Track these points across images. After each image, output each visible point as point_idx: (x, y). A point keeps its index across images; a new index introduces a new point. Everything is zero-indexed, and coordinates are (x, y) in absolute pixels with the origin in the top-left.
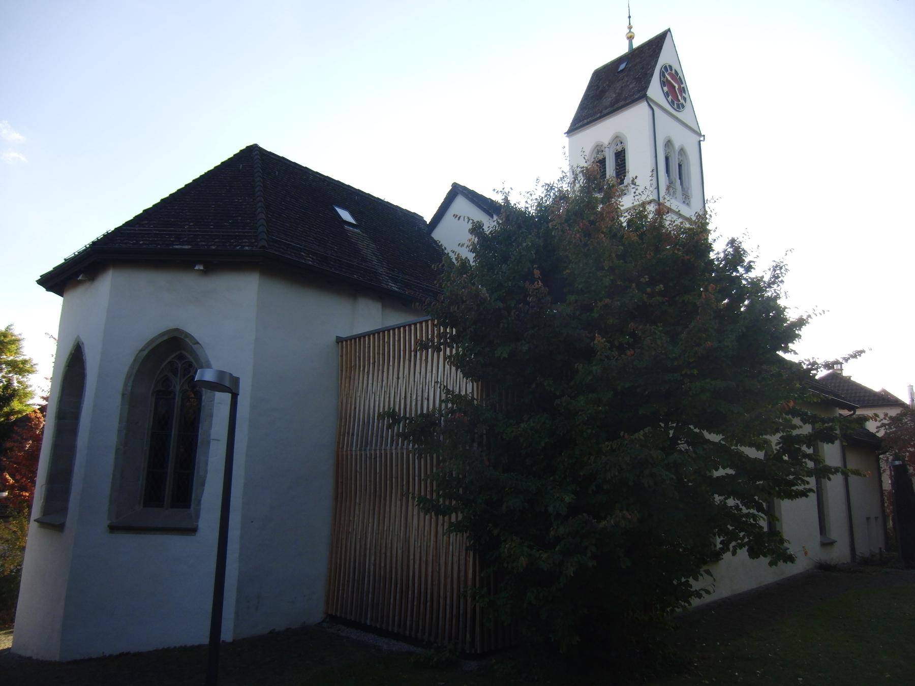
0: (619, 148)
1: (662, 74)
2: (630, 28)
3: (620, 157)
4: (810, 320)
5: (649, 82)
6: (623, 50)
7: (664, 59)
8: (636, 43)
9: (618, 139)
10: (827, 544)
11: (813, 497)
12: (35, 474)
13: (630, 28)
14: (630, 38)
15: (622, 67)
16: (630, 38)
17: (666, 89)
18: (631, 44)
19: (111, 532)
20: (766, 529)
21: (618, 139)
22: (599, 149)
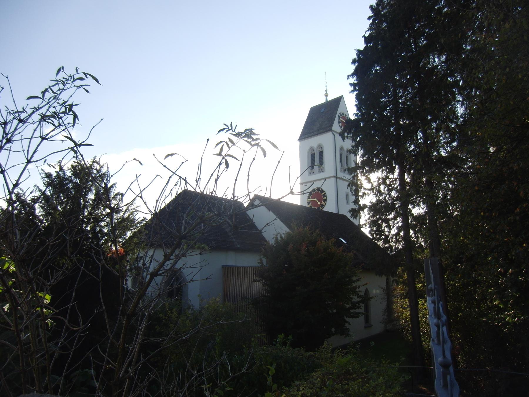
0: (321, 150)
1: (339, 118)
2: (326, 91)
3: (321, 154)
4: (88, 156)
5: (333, 123)
6: (323, 101)
7: (340, 111)
8: (329, 99)
9: (320, 147)
10: (198, 180)
11: (362, 318)
12: (430, 276)
13: (326, 91)
14: (326, 95)
15: (323, 110)
16: (326, 95)
17: (340, 124)
18: (327, 99)
19: (370, 8)
20: (345, 318)
21: (320, 147)
22: (312, 149)
